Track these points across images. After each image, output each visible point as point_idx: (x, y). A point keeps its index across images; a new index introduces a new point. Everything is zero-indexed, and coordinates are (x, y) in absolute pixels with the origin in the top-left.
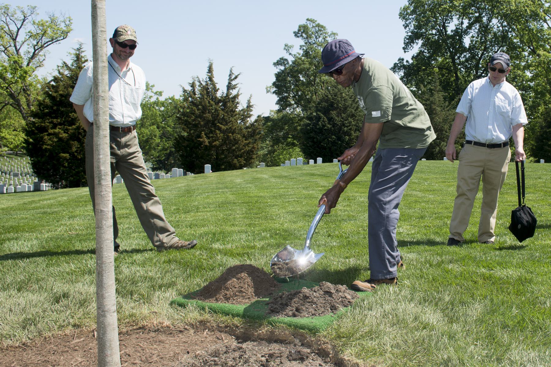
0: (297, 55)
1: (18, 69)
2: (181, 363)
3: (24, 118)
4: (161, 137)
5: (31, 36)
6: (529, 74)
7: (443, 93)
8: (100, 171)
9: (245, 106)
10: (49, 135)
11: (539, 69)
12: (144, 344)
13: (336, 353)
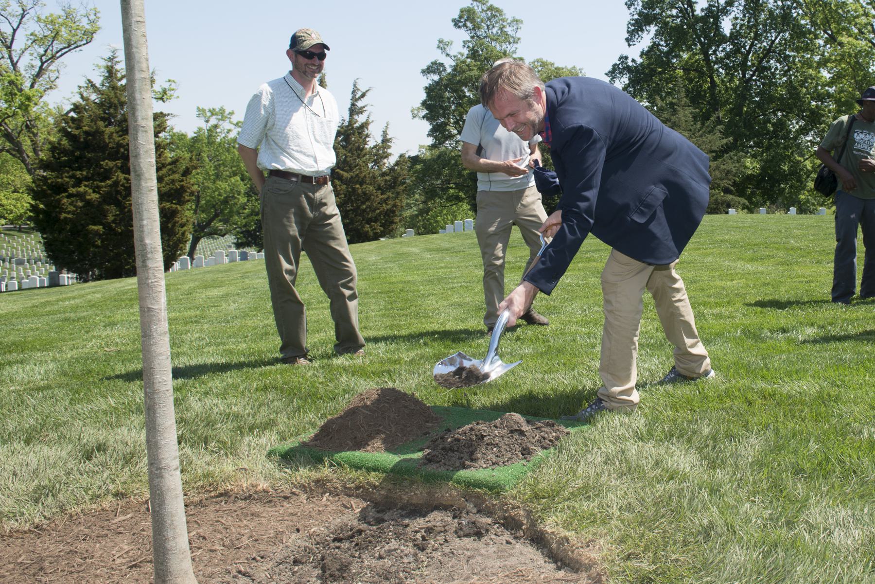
0: (459, 56)
1: (16, 94)
2: (287, 547)
3: (29, 171)
4: (248, 195)
5: (34, 41)
6: (826, 74)
7: (691, 109)
8: (144, 246)
9: (379, 140)
10: (70, 196)
11: (843, 66)
12: (227, 520)
13: (533, 523)
